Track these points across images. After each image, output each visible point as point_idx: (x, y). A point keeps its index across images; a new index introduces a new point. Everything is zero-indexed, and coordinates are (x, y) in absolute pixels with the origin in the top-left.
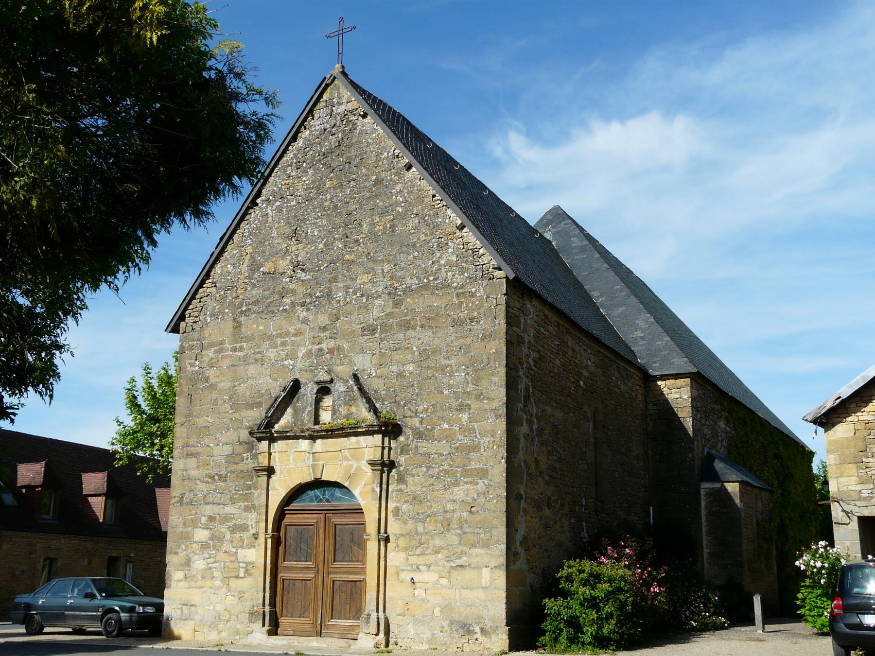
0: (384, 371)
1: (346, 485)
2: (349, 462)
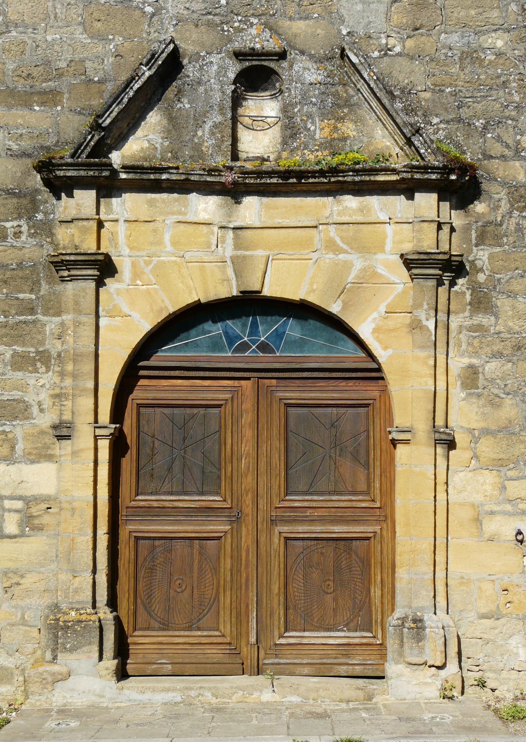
0: (425, 42)
1: (335, 308)
2: (348, 256)
